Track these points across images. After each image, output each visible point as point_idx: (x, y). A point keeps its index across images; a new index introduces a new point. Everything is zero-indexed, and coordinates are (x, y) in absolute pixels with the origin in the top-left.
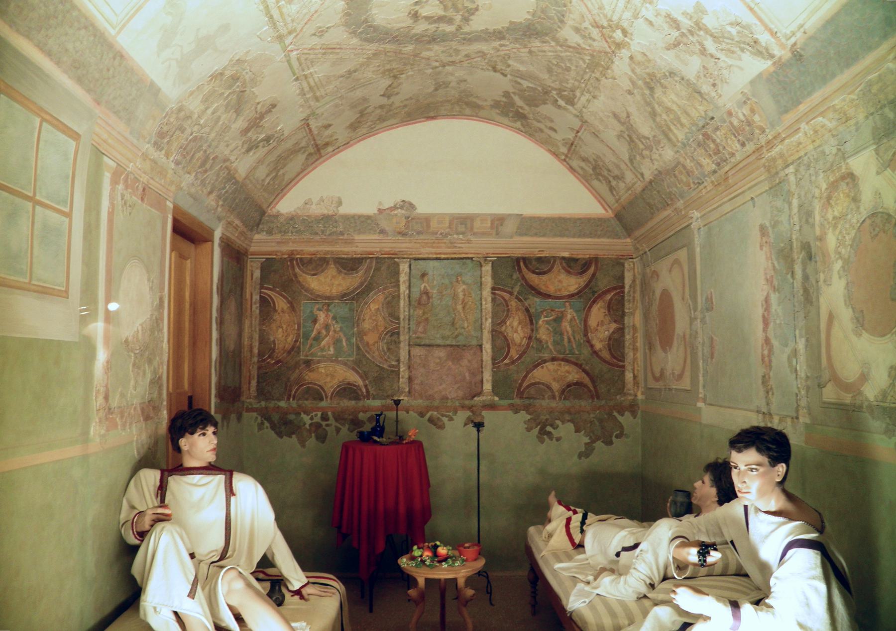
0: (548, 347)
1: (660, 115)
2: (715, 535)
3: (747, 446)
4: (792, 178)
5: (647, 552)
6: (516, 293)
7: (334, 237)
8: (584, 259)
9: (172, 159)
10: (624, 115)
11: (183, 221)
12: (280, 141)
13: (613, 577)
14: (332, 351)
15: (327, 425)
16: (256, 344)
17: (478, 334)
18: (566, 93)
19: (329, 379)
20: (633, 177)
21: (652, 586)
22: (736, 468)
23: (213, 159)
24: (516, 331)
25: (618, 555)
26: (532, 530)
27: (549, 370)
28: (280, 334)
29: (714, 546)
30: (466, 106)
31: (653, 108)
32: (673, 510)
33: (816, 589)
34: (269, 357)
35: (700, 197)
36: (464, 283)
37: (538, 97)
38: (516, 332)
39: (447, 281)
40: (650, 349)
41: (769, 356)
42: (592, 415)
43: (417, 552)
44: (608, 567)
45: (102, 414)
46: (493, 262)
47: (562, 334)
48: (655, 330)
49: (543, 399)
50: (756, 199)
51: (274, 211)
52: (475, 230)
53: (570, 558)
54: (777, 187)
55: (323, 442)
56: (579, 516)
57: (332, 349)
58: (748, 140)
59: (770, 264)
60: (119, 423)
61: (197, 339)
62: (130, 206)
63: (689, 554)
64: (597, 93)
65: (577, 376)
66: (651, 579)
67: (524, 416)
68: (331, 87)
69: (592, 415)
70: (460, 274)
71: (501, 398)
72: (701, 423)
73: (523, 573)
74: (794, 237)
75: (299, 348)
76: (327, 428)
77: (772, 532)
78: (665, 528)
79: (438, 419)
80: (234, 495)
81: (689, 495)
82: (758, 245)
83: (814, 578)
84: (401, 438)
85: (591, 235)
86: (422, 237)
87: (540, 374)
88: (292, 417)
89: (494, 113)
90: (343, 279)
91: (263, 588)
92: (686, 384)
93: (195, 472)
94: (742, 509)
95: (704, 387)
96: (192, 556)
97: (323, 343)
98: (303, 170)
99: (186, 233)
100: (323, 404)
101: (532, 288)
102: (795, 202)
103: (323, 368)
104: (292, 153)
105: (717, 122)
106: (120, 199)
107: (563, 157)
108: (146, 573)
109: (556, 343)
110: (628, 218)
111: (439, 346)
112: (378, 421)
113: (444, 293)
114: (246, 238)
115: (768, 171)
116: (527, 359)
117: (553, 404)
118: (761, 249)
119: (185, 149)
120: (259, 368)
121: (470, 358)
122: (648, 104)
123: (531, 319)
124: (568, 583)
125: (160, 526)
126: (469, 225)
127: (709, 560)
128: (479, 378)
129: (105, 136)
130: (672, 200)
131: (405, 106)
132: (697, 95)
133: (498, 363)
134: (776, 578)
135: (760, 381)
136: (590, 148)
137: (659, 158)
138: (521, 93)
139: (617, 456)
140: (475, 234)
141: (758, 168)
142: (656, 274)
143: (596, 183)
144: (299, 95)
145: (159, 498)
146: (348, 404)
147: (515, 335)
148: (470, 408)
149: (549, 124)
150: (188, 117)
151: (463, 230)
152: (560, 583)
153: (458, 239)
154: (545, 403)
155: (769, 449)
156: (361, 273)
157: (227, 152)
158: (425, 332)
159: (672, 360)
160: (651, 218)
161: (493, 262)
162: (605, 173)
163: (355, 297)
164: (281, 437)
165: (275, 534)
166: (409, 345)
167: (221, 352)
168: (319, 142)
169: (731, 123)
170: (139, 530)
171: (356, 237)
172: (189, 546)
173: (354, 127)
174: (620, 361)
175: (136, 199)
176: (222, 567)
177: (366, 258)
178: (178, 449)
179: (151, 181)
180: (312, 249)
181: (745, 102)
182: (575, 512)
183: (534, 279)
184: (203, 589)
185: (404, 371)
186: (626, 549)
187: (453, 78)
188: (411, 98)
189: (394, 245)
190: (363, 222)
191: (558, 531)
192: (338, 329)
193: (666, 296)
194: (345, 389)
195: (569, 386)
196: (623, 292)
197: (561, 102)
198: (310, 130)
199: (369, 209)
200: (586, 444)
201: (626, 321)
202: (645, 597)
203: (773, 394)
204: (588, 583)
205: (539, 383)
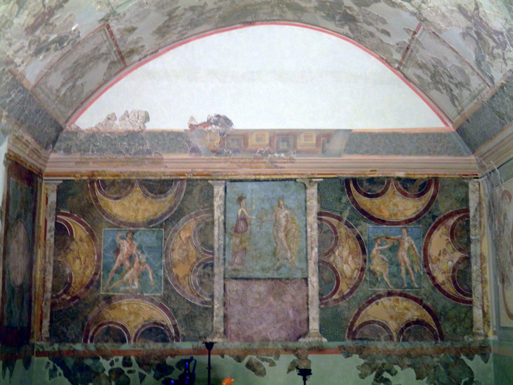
0: (383, 279)
6: (345, 219)
7: (141, 157)
8: (422, 179)
12: (76, 44)
14: (136, 285)
15: (130, 372)
17: (304, 266)
19: (132, 318)
20: (480, 82)
24: (346, 262)
28: (77, 266)
34: (65, 292)
36: (286, 207)
38: (346, 262)
39: (267, 206)
40: (503, 281)
42: (436, 359)
46: (319, 184)
47: (398, 265)
49: (379, 340)
52: (299, 148)
57: (136, 283)
67: (356, 360)
70: (282, 198)
71: (330, 340)
75: (99, 282)
79: (258, 364)
86: (238, 156)
88: (89, 362)
89: (319, 17)
90: (151, 203)
97: (127, 276)
98: (105, 82)
100: (125, 347)
101: (364, 212)
103: (125, 305)
104: (91, 61)
107: (397, 65)
109: (392, 275)
110: (469, 134)
111: (258, 279)
112: (187, 368)
113: (264, 219)
114: (39, 157)
116: (359, 294)
117: (391, 346)
120: (53, 305)
121: (294, 293)
123: (363, 247)
126: (292, 143)
128: (304, 316)
131: (219, 9)
133: (327, 298)
136: (429, 51)
140: (298, 152)
143: (434, 93)
146: (154, 346)
147: (345, 267)
148: (295, 351)
149: (381, 26)
151: (286, 147)
153: (279, 158)
154: (381, 345)
158: (242, 263)
161: (319, 184)
162: (446, 80)
166: (225, 278)
168: (122, 49)
171: (165, 156)
173: (162, 31)
177: (176, 180)
183: (365, 202)
185: (218, 309)
190: (173, 140)
192: (144, 260)
194: (150, 330)
195: (408, 324)
196: (468, 216)
198: (112, 34)
199: (180, 125)
205: (374, 322)
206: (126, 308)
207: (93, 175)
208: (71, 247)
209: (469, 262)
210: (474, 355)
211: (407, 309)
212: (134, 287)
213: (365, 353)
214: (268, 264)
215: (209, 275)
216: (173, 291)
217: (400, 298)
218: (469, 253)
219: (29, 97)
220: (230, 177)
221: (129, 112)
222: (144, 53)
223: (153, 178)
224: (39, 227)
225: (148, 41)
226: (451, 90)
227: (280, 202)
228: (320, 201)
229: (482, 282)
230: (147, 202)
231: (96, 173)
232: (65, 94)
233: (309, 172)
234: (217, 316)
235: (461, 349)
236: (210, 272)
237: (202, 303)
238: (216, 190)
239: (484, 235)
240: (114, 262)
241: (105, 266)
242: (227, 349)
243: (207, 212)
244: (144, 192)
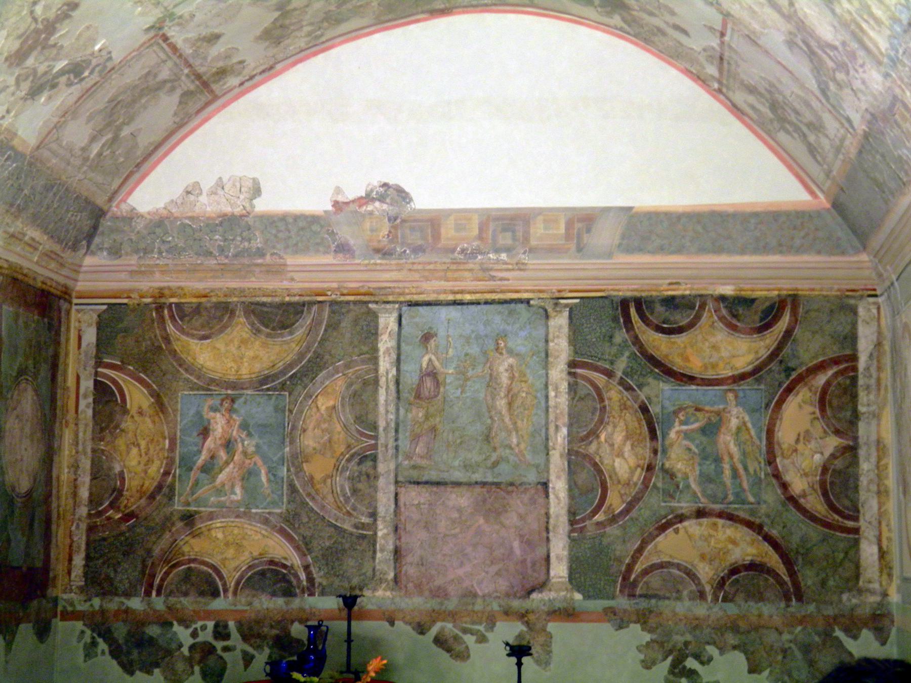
0: (688, 487)
6: (619, 374)
7: (246, 261)
8: (767, 298)
14: (238, 494)
15: (226, 649)
16: (85, 480)
17: (540, 459)
19: (230, 553)
28: (133, 460)
34: (112, 506)
36: (511, 352)
39: (475, 350)
42: (786, 637)
47: (718, 460)
49: (679, 599)
52: (533, 243)
57: (238, 490)
69: (786, 637)
70: (504, 335)
71: (587, 597)
75: (172, 488)
76: (226, 655)
79: (456, 638)
85: (780, 248)
86: (422, 258)
87: (669, 546)
88: (153, 631)
90: (264, 345)
97: (222, 477)
98: (180, 126)
100: (218, 604)
104: (141, 95)
107: (716, 86)
109: (706, 479)
111: (457, 484)
113: (470, 374)
116: (643, 512)
117: (701, 610)
120: (91, 529)
121: (522, 510)
123: (652, 427)
126: (520, 234)
128: (541, 552)
133: (583, 520)
136: (754, 69)
140: (532, 250)
143: (782, 136)
146: (269, 604)
148: (522, 616)
151: (509, 242)
153: (498, 261)
158: (428, 455)
164: (131, 673)
166: (397, 482)
168: (201, 70)
171: (291, 260)
173: (274, 35)
180: (201, 286)
185: (385, 536)
190: (303, 229)
194: (262, 573)
195: (734, 571)
196: (855, 369)
198: (174, 48)
199: (315, 202)
205: (669, 564)
206: (220, 535)
207: (162, 295)
208: (123, 426)
209: (855, 457)
210: (860, 630)
211: (734, 542)
212: (234, 497)
213: (653, 621)
214: (475, 457)
215: (368, 476)
216: (304, 504)
217: (721, 522)
218: (855, 439)
220: (408, 298)
221: (225, 180)
222: (247, 73)
224: (66, 389)
225: (253, 55)
226: (805, 136)
228: (574, 340)
231: (166, 292)
232: (100, 154)
233: (554, 286)
234: (382, 550)
235: (835, 618)
236: (371, 472)
238: (382, 321)
239: (885, 405)
240: (200, 452)
241: (182, 459)
243: (363, 362)
244: (252, 325)
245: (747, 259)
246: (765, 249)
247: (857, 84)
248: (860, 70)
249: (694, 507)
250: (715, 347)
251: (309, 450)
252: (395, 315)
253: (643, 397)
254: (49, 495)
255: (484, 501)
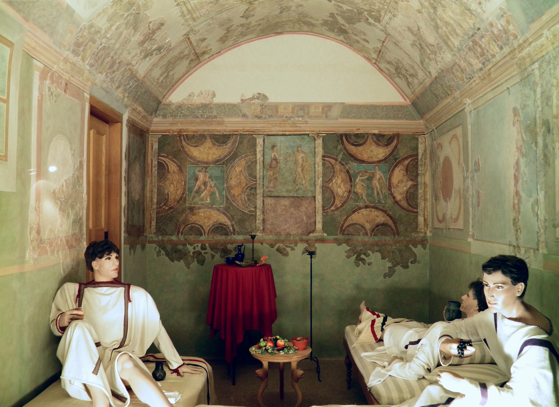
0: (362, 198)
1: (442, 28)
2: (472, 334)
3: (495, 269)
4: (537, 72)
5: (426, 346)
6: (340, 160)
7: (210, 120)
8: (389, 135)
9: (87, 62)
10: (416, 29)
11: (98, 107)
12: (169, 50)
13: (402, 363)
14: (209, 200)
15: (205, 253)
16: (155, 196)
17: (313, 189)
18: (374, 13)
19: (206, 220)
20: (424, 74)
21: (429, 370)
22: (487, 285)
23: (119, 63)
24: (340, 188)
25: (406, 347)
26: (348, 328)
27: (363, 215)
28: (172, 189)
29: (469, 343)
30: (303, 24)
31: (436, 23)
32: (447, 316)
33: (545, 376)
34: (165, 204)
35: (471, 89)
36: (302, 152)
37: (354, 17)
39: (290, 151)
40: (436, 200)
41: (518, 204)
42: (394, 247)
43: (262, 343)
44: (399, 356)
45: (35, 243)
46: (323, 137)
47: (373, 189)
48: (440, 186)
49: (359, 235)
50: (511, 89)
51: (167, 101)
52: (311, 114)
53: (373, 349)
54: (526, 79)
55: (202, 265)
56: (381, 319)
57: (208, 199)
58: (505, 44)
59: (520, 136)
60: (49, 249)
61: (111, 191)
62: (55, 96)
63: (451, 348)
64: (396, 13)
65: (383, 219)
66: (428, 365)
67: (345, 247)
68: (204, 10)
69: (394, 247)
70: (300, 146)
71: (328, 235)
72: (470, 253)
73: (343, 359)
74: (538, 116)
75: (185, 198)
76: (205, 255)
77: (513, 333)
78: (439, 328)
79: (284, 249)
80: (130, 301)
81: (459, 304)
82: (512, 123)
83: (543, 368)
84: (256, 262)
85: (394, 118)
86: (272, 119)
87: (357, 218)
88: (180, 247)
89: (324, 29)
90: (217, 149)
91: (149, 369)
92: (460, 225)
93: (103, 285)
94: (493, 316)
95: (473, 227)
96: (98, 345)
97: (203, 195)
98: (188, 72)
99: (100, 116)
100: (202, 238)
102: (539, 90)
104: (178, 60)
105: (482, 32)
106: (47, 90)
107: (374, 61)
108: (65, 356)
109: (368, 195)
111: (284, 197)
112: (240, 250)
113: (288, 159)
114: (147, 121)
115: (520, 67)
116: (347, 206)
117: (366, 239)
118: (514, 126)
119: (96, 55)
120: (157, 213)
121: (307, 206)
122: (433, 20)
123: (351, 178)
124: (370, 367)
125: (74, 323)
126: (306, 111)
127: (466, 353)
128: (313, 220)
129: (34, 45)
130: (451, 91)
131: (259, 25)
132: (467, 12)
133: (327, 209)
134: (515, 367)
135: (512, 223)
136: (393, 54)
137: (441, 60)
138: (343, 14)
139: (411, 276)
140: (310, 117)
141: (512, 66)
142: (440, 146)
143: (397, 80)
144: (181, 16)
145: (77, 303)
146: (220, 238)
148: (306, 241)
149: (363, 37)
150: (97, 32)
151: (302, 114)
152: (364, 367)
153: (298, 121)
154: (360, 238)
155: (511, 272)
156: (229, 145)
157: (129, 58)
158: (274, 187)
159: (451, 208)
160: (437, 105)
161: (323, 137)
162: (404, 72)
163: (224, 163)
164: (173, 261)
165: (161, 329)
166: (263, 196)
167: (128, 201)
168: (197, 51)
169: (493, 32)
170: (61, 326)
171: (226, 120)
172: (96, 337)
173: (223, 40)
174: (414, 208)
175: (60, 91)
176: (120, 352)
177: (232, 134)
178: (92, 269)
179: (72, 78)
180: (194, 128)
181: (502, 16)
182: (378, 316)
183: (352, 149)
184: (105, 369)
185: (259, 215)
186: (412, 343)
187: (292, 3)
188: (263, 19)
189: (252, 125)
190: (230, 109)
191: (366, 329)
193: (447, 161)
194: (217, 228)
195: (377, 226)
196: (417, 159)
197: (371, 20)
198: (191, 43)
199: (235, 100)
200: (389, 267)
201: (419, 180)
202: (424, 378)
203: (521, 232)
204: (384, 367)
205: (356, 224)
206: (202, 215)
207: (180, 132)
208: (168, 177)
209: (417, 188)
210: (417, 245)
211: (377, 216)
212: (207, 202)
213: (350, 243)
214: (290, 188)
215: (253, 194)
216: (231, 204)
217: (373, 210)
218: (417, 182)
219: (140, 83)
220: (267, 133)
221: (203, 91)
222: (212, 53)
223: (218, 133)
224: (148, 164)
225: (214, 46)
226: (407, 79)
227: (298, 149)
228: (324, 148)
229: (424, 200)
230: (214, 149)
231: (182, 131)
232: (162, 81)
233: (317, 130)
234: (259, 220)
235: (410, 241)
236: (254, 193)
237: (249, 211)
238: (258, 141)
239: (427, 171)
240: (195, 186)
241: (189, 188)
242: (265, 240)
243: (252, 155)
244: (213, 142)
245: (383, 121)
246: (389, 118)
247: (439, 59)
248: (442, 54)
249: (364, 205)
250: (372, 151)
251: (233, 185)
252: (262, 139)
253: (347, 168)
254: (144, 201)
255: (294, 203)
